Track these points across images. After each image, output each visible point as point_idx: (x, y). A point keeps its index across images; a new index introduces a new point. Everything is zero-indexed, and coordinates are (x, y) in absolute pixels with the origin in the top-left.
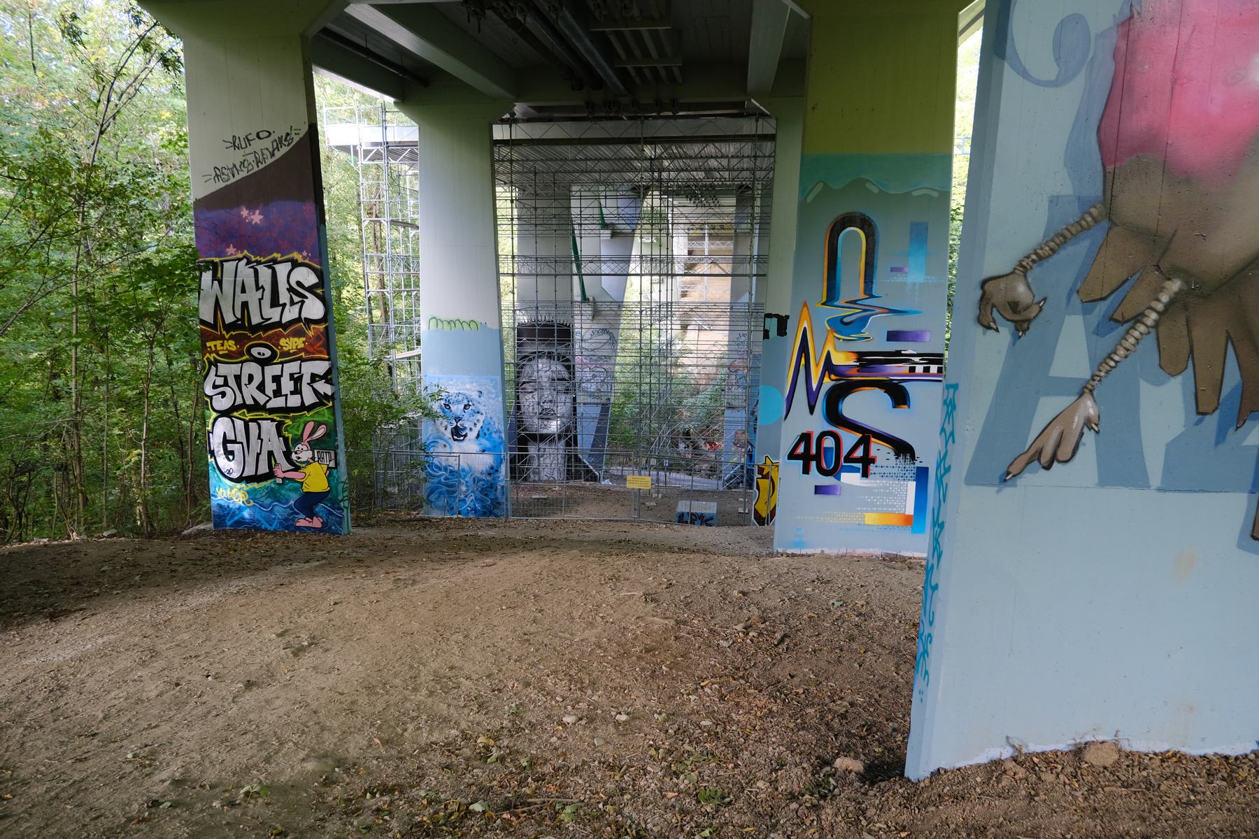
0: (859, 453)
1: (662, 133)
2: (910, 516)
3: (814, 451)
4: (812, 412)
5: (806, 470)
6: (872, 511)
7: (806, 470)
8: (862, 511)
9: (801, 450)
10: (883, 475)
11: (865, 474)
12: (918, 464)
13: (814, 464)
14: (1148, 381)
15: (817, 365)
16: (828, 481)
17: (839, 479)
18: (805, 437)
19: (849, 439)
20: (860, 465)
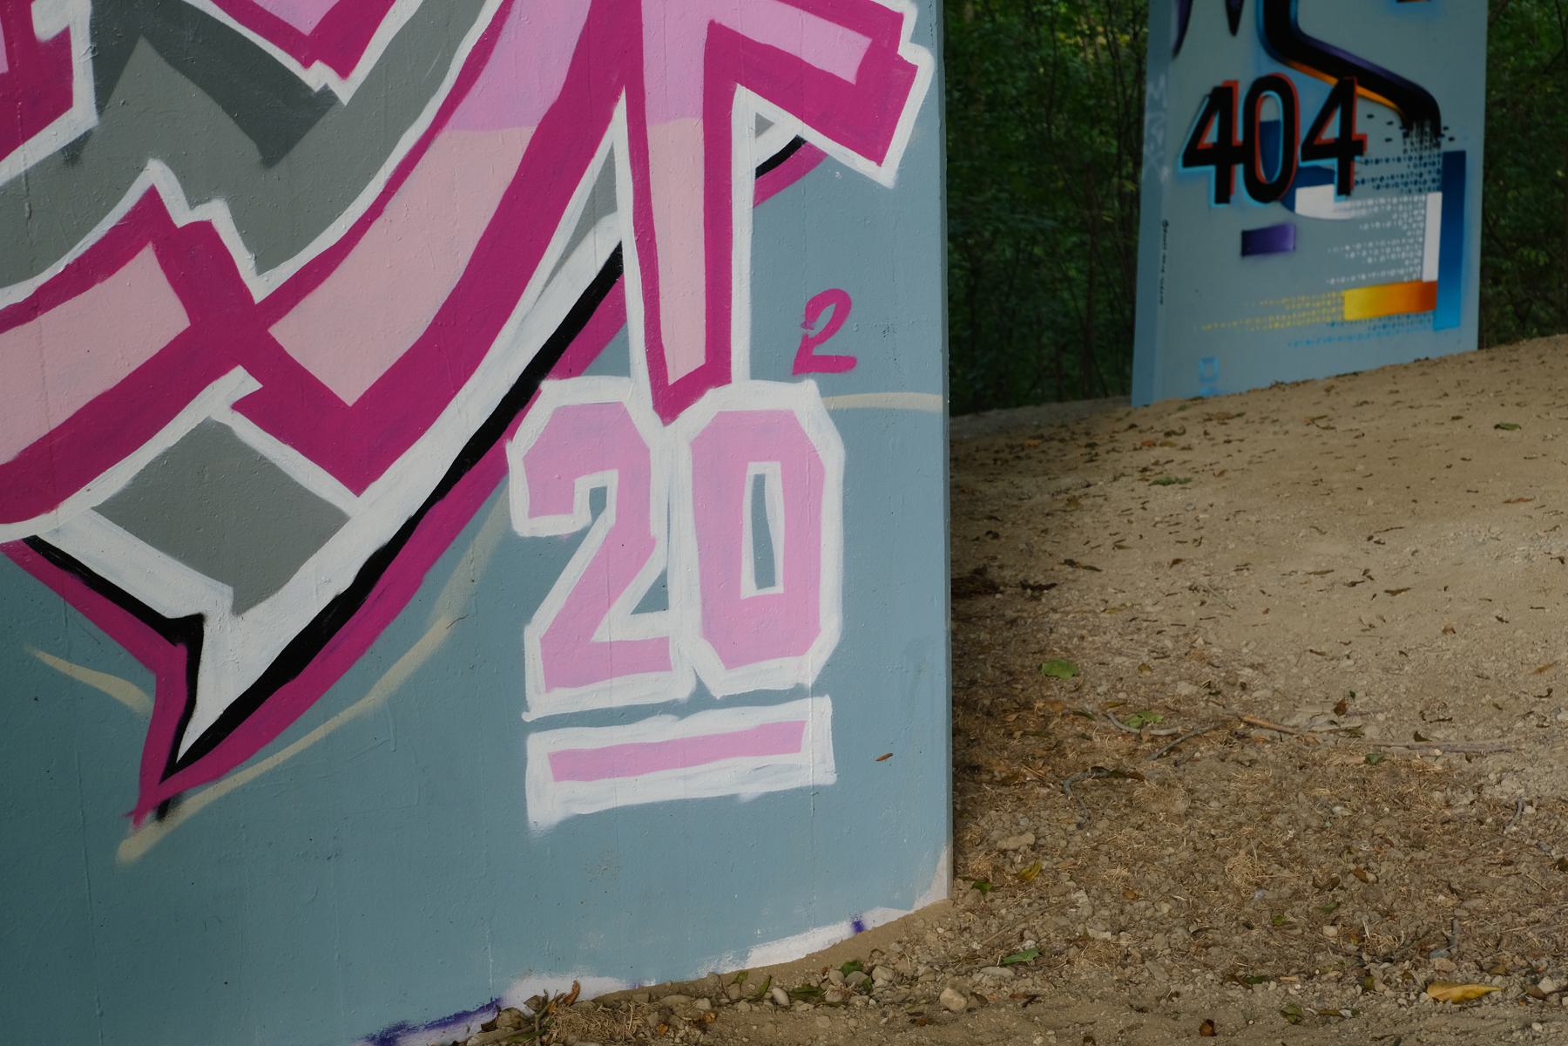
0: (1332, 131)
1: (619, 701)
2: (1431, 285)
3: (1239, 136)
4: (1234, 27)
5: (1223, 194)
6: (1358, 285)
7: (1223, 194)
8: (1338, 288)
9: (1211, 136)
10: (1380, 184)
11: (1344, 189)
12: (1447, 146)
13: (1239, 170)
14: (160, 257)
15: (611, 155)
16: (1266, 215)
17: (1290, 204)
18: (1221, 98)
19: (1313, 91)
20: (1331, 163)
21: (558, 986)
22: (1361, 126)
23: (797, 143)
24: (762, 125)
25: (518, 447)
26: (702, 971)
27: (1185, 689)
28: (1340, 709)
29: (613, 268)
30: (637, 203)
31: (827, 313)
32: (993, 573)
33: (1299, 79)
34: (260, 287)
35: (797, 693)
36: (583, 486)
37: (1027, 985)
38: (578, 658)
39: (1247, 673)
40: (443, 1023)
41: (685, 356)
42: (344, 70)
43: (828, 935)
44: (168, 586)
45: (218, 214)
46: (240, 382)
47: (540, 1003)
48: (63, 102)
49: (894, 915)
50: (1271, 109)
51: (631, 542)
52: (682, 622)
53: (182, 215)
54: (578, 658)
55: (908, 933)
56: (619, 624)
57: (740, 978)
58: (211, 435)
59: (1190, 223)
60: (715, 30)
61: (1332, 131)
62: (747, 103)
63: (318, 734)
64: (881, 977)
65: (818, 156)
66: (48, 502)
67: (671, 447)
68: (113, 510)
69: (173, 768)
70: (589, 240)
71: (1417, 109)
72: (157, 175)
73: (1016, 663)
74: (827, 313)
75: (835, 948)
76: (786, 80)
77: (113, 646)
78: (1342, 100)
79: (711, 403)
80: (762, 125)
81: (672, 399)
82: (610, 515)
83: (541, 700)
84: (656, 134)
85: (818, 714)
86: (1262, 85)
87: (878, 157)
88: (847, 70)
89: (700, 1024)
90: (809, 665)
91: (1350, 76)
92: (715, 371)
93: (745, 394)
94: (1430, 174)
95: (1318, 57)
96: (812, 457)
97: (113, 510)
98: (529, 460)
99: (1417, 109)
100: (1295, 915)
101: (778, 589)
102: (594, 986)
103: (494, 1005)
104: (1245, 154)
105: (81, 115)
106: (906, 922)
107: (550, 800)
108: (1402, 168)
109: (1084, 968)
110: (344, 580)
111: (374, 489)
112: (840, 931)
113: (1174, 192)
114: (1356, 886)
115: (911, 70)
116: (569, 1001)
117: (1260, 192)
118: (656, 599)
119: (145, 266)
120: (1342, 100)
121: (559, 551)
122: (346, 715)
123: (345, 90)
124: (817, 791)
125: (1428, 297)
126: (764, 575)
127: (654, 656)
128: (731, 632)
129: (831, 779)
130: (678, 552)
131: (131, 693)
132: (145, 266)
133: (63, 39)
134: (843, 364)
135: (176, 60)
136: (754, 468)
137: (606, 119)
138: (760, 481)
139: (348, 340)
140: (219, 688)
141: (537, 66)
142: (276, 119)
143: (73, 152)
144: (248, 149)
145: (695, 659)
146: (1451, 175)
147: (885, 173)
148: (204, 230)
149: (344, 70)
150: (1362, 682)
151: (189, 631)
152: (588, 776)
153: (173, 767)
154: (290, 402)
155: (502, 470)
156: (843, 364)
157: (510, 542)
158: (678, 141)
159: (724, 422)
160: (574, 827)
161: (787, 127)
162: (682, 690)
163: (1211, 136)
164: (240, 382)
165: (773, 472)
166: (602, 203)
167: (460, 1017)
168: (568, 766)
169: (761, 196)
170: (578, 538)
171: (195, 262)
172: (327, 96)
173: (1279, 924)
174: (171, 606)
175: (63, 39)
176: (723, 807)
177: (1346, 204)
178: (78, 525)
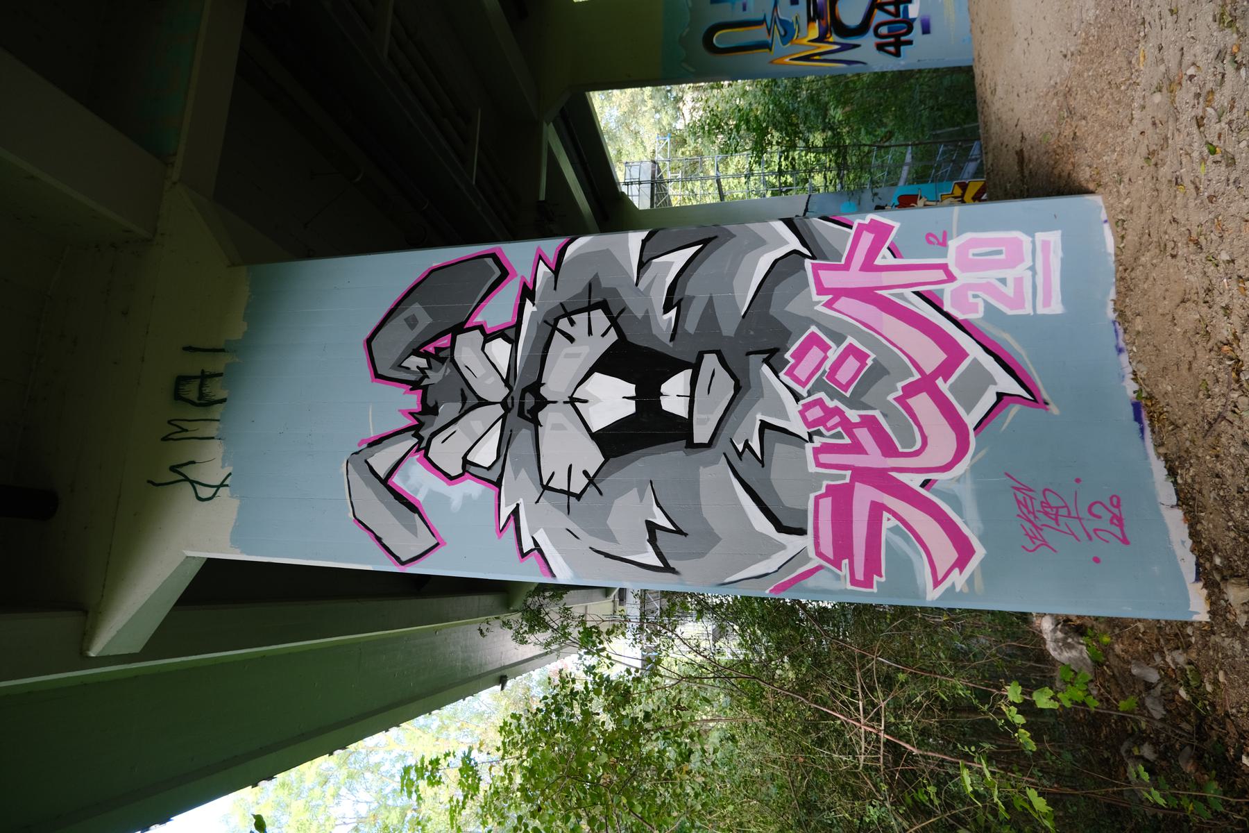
0: (891, 8)
3: (892, 40)
5: (910, 43)
7: (910, 43)
9: (892, 49)
13: (903, 38)
16: (917, 27)
17: (914, 20)
18: (880, 47)
21: (1111, 305)
24: (884, 257)
26: (1113, 266)
27: (1055, 103)
28: (1065, 56)
29: (917, 293)
30: (900, 288)
32: (1018, 149)
33: (875, 22)
34: (917, 376)
35: (1033, 243)
36: (972, 300)
37: (1126, 180)
39: (1052, 82)
40: (1117, 336)
41: (940, 275)
42: (868, 356)
43: (1107, 229)
44: (989, 399)
45: (900, 385)
46: (940, 382)
47: (1115, 310)
48: (874, 417)
49: (1104, 211)
51: (988, 288)
52: (1010, 274)
53: (900, 393)
54: (1018, 301)
55: (1109, 208)
56: (1009, 291)
57: (1116, 255)
58: (951, 389)
59: (921, 53)
62: (879, 261)
63: (1030, 366)
64: (1121, 217)
65: (892, 243)
66: (965, 425)
67: (962, 278)
68: (968, 411)
69: (1035, 400)
72: (891, 398)
73: (1043, 150)
75: (1111, 228)
76: (873, 251)
77: (1001, 414)
79: (954, 269)
80: (884, 257)
81: (951, 278)
83: (1028, 310)
84: (885, 284)
85: (1040, 236)
86: (877, 34)
87: (892, 227)
89: (1125, 270)
90: (1026, 239)
92: (944, 267)
93: (951, 260)
95: (869, 16)
96: (971, 240)
97: (968, 411)
100: (1117, 96)
101: (1004, 249)
102: (1112, 295)
103: (1114, 322)
104: (897, 37)
105: (877, 413)
106: (1106, 208)
107: (1056, 308)
109: (1124, 163)
112: (1107, 227)
113: (910, 58)
114: (1111, 77)
116: (1115, 302)
117: (910, 30)
118: (1003, 281)
119: (912, 402)
123: (873, 356)
124: (1062, 235)
126: (1000, 252)
127: (1019, 281)
128: (1013, 261)
131: (1014, 409)
132: (912, 402)
133: (861, 416)
134: (945, 234)
135: (865, 393)
136: (971, 256)
137: (882, 296)
139: (931, 357)
140: (1015, 389)
141: (869, 312)
142: (879, 371)
143: (885, 415)
144: (886, 377)
145: (1021, 270)
147: (897, 225)
148: (904, 388)
149: (868, 356)
150: (1058, 48)
151: (1000, 396)
152: (1050, 297)
153: (1035, 401)
154: (945, 370)
155: (966, 321)
156: (945, 234)
159: (958, 265)
160: (1065, 301)
161: (885, 251)
162: (1030, 273)
164: (940, 382)
165: (972, 251)
166: (901, 296)
167: (1116, 331)
168: (1047, 303)
169: (901, 257)
171: (911, 390)
172: (874, 360)
173: (1119, 102)
174: (994, 399)
175: (861, 416)
178: (971, 420)
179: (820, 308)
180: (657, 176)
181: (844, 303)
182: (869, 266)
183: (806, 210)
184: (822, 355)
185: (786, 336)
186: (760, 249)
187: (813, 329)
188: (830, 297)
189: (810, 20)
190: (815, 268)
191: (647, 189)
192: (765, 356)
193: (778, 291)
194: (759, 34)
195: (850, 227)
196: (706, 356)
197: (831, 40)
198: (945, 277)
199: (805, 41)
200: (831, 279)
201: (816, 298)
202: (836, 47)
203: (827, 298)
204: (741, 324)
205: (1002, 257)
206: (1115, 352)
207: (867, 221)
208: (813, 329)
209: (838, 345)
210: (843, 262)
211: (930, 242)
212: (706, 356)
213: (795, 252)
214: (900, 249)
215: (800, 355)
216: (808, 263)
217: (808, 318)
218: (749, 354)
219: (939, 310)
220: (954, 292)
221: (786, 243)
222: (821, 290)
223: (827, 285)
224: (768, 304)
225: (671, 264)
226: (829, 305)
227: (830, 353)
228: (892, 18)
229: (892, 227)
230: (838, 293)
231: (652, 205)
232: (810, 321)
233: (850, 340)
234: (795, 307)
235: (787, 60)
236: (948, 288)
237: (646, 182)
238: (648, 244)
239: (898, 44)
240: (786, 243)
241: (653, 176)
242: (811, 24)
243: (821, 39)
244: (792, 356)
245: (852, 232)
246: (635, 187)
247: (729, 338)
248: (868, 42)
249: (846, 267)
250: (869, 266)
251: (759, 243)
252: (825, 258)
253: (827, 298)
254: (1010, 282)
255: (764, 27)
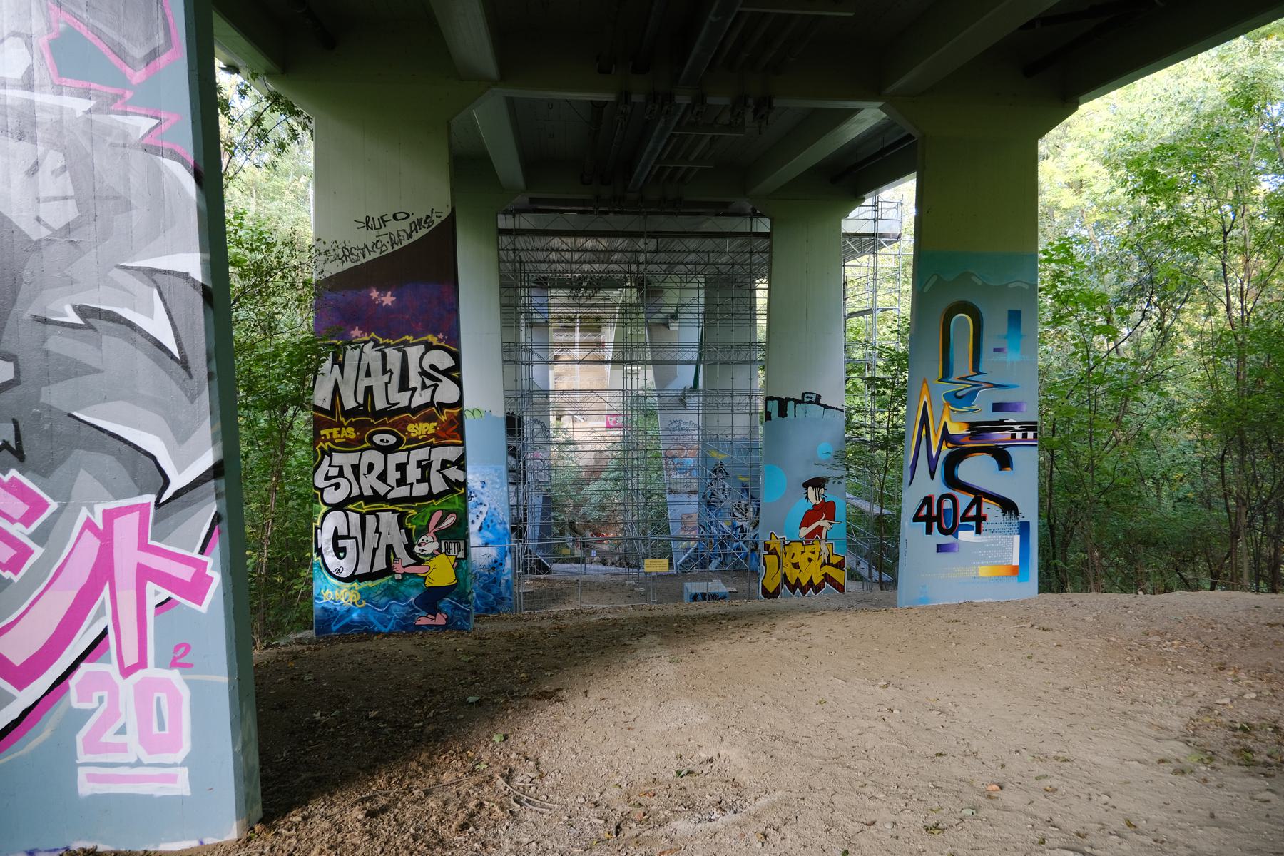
0: (973, 512)
3: (935, 513)
4: (932, 478)
5: (929, 531)
7: (929, 531)
9: (924, 512)
11: (978, 532)
12: (1021, 519)
13: (935, 524)
15: (103, 602)
18: (928, 501)
19: (964, 500)
20: (973, 523)
22: (984, 512)
23: (169, 599)
24: (157, 593)
25: (73, 681)
30: (114, 611)
31: (182, 650)
33: (957, 494)
35: (175, 765)
36: (96, 695)
38: (94, 745)
41: (131, 658)
42: (16, 572)
50: (948, 504)
51: (112, 714)
52: (132, 738)
56: (109, 737)
59: (916, 541)
60: (139, 565)
61: (973, 512)
62: (151, 587)
65: (177, 603)
67: (127, 686)
70: (96, 624)
71: (1008, 506)
74: (182, 650)
76: (164, 580)
78: (977, 502)
79: (139, 675)
80: (157, 593)
81: (126, 672)
82: (105, 704)
83: (82, 757)
85: (184, 773)
87: (200, 604)
88: (188, 578)
90: (180, 756)
91: (979, 495)
92: (142, 664)
93: (151, 671)
94: (1016, 528)
95: (966, 488)
96: (181, 699)
98: (77, 686)
99: (1008, 506)
101: (167, 732)
107: (86, 788)
108: (1003, 526)
110: (16, 716)
111: (25, 690)
112: (195, 843)
113: (912, 532)
115: (211, 579)
117: (944, 532)
120: (977, 502)
121: (88, 714)
122: (17, 754)
123: (16, 579)
125: (1015, 571)
126: (161, 726)
128: (146, 740)
129: (189, 794)
130: (129, 716)
137: (102, 589)
138: (159, 699)
141: (79, 573)
145: (136, 750)
146: (1024, 528)
147: (203, 608)
149: (16, 572)
155: (67, 688)
157: (71, 710)
158: (127, 598)
159: (145, 680)
160: (94, 797)
161: (165, 594)
162: (133, 760)
163: (924, 512)
165: (164, 697)
166: (101, 613)
168: (92, 778)
169: (157, 613)
170: (94, 711)
172: (10, 581)
176: (148, 798)
177: (978, 537)
179: (84, 514)
180: (882, 241)
181: (92, 545)
182: (144, 574)
183: (826, 407)
184: (17, 517)
185: (43, 471)
186: (170, 436)
187: (53, 506)
188: (101, 526)
189: (971, 425)
190: (143, 508)
191: (868, 228)
192: (13, 444)
193: (108, 460)
194: (962, 365)
195: (202, 551)
196: (11, 365)
197: (944, 447)
198: (127, 664)
199: (946, 419)
200: (126, 529)
201: (99, 509)
202: (934, 454)
203: (99, 522)
204: (59, 412)
205: (155, 730)
206: (30, 847)
207: (209, 572)
208: (53, 506)
209: (31, 537)
210: (150, 542)
211: (177, 648)
212: (11, 365)
213: (167, 482)
214: (166, 614)
215: (16, 489)
216: (150, 499)
217: (68, 499)
218: (15, 422)
219: (82, 658)
220: (107, 675)
221: (180, 469)
222: (109, 516)
223: (118, 523)
224: (90, 447)
225: (150, 315)
226: (89, 525)
227: (19, 526)
228: (961, 513)
229: (200, 604)
230: (106, 537)
231: (847, 234)
232: (66, 500)
233: (38, 551)
234: (85, 481)
235: (925, 399)
236: (113, 669)
237: (876, 227)
238: (180, 282)
239: (929, 520)
240: (180, 469)
241: (882, 235)
242: (966, 426)
243: (946, 436)
244: (13, 478)
245: (195, 554)
246: (870, 215)
247: (38, 395)
248: (937, 487)
249: (143, 546)
250: (144, 574)
251: (180, 434)
252: (156, 521)
253: (99, 522)
254: (120, 739)
255: (969, 371)
